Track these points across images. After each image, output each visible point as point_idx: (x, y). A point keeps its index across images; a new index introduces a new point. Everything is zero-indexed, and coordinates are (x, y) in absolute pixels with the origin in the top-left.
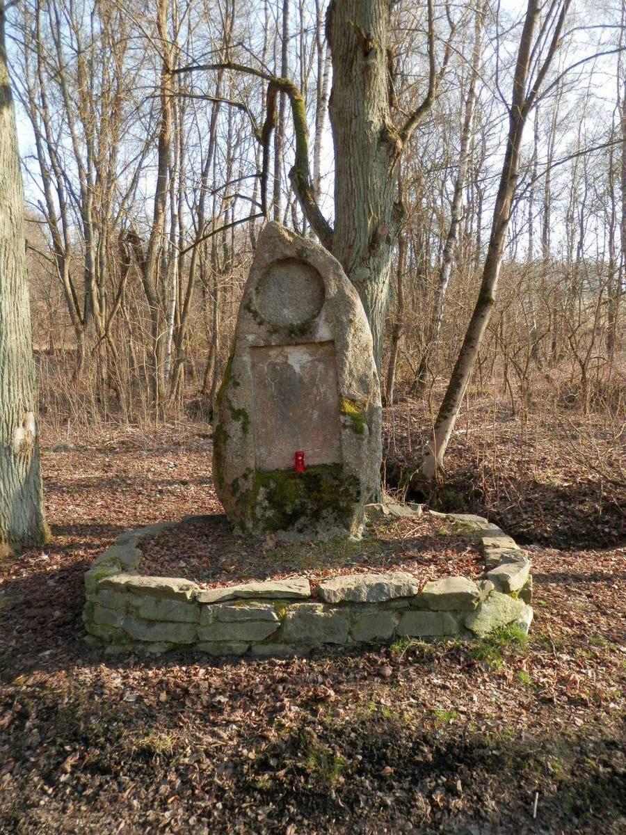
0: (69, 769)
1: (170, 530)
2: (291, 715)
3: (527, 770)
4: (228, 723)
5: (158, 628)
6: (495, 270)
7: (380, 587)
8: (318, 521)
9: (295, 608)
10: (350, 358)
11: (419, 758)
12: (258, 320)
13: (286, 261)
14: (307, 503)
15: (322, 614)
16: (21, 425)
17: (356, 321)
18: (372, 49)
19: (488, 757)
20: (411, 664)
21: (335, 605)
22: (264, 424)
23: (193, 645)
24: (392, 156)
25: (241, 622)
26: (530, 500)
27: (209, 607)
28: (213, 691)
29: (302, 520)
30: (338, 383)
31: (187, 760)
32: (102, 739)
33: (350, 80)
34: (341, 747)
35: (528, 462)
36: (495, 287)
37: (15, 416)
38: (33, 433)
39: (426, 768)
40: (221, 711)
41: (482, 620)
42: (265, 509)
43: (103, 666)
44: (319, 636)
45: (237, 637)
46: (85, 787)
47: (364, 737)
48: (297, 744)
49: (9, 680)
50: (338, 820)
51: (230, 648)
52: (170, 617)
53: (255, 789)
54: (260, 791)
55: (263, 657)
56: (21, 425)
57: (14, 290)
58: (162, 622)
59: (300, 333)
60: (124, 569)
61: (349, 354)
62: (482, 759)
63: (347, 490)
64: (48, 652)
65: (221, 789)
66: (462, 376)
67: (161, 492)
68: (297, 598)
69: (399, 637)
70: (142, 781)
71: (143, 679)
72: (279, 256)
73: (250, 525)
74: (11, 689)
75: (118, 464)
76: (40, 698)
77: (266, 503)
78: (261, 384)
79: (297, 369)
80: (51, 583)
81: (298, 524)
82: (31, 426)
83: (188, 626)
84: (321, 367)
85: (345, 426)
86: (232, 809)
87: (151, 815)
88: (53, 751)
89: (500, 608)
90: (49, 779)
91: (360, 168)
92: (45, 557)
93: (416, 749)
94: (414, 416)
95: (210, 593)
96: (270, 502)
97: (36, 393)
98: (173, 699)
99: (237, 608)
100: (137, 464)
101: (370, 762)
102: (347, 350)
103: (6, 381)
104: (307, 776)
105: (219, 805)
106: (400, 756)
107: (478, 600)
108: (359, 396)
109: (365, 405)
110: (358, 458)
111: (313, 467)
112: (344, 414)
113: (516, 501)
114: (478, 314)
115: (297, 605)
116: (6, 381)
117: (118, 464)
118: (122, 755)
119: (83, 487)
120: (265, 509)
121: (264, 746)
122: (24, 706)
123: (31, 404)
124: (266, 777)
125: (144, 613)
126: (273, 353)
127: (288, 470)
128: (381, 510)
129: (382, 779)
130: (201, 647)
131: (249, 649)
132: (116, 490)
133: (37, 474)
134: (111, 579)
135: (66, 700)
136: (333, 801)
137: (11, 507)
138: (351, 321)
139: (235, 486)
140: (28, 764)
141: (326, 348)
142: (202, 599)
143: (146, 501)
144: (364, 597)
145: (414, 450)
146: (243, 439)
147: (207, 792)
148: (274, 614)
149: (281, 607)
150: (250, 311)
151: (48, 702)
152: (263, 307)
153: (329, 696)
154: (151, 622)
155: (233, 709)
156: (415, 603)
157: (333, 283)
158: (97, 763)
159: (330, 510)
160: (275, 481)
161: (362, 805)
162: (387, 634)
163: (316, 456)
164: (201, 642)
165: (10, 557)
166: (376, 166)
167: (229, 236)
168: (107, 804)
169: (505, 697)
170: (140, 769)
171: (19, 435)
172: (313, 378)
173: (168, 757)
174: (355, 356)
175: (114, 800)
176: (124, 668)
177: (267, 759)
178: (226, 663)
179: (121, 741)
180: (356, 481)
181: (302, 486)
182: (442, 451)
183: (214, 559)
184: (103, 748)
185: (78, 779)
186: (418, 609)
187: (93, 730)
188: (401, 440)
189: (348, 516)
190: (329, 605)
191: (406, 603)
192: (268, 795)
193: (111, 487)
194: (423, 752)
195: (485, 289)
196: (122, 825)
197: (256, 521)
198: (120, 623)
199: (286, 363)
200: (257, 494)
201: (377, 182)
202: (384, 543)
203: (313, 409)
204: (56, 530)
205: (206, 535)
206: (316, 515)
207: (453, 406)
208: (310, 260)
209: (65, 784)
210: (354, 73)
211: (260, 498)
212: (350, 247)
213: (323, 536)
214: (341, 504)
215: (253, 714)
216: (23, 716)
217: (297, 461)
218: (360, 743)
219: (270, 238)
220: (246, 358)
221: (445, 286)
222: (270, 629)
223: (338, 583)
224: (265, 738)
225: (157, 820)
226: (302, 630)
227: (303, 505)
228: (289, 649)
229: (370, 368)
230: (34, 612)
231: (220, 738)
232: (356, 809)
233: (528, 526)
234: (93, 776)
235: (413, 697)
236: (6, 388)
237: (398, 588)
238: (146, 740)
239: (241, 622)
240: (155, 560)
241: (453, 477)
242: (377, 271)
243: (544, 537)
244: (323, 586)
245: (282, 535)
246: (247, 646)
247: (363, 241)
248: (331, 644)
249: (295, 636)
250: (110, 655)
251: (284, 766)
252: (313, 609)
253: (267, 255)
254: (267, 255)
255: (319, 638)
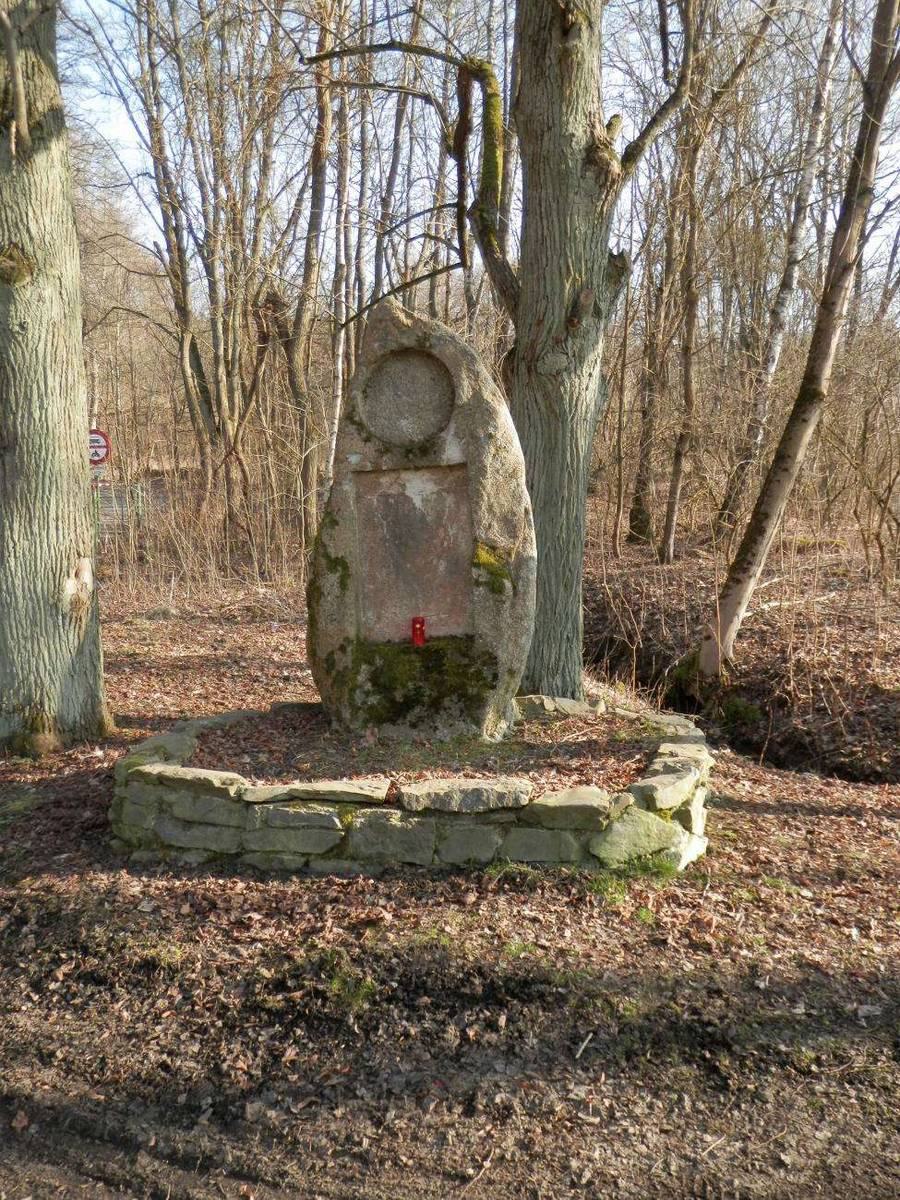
0: (61, 978)
1: (250, 719)
2: (330, 936)
3: (591, 1010)
4: (254, 940)
5: (196, 831)
6: (828, 345)
7: (477, 792)
8: (437, 712)
9: (364, 815)
10: (488, 487)
11: (467, 991)
12: (364, 435)
13: (403, 353)
14: (423, 686)
15: (399, 824)
16: (72, 575)
17: (499, 436)
18: (573, 24)
19: (551, 994)
20: (505, 893)
21: (417, 813)
22: (372, 578)
23: (238, 855)
24: (604, 184)
25: (293, 828)
26: (861, 714)
27: (256, 807)
28: (246, 907)
29: (417, 710)
30: (473, 522)
31: (194, 976)
32: (103, 949)
33: (543, 73)
34: (374, 971)
35: (869, 655)
36: (827, 372)
37: (65, 563)
38: (90, 587)
39: (471, 1001)
40: (248, 928)
41: (612, 844)
42: (367, 694)
43: (123, 872)
44: (394, 852)
45: (291, 847)
46: (74, 995)
47: (408, 964)
48: (324, 966)
49: (13, 882)
50: (347, 1045)
51: (282, 862)
52: (212, 817)
53: (263, 1009)
54: (269, 1011)
55: (320, 875)
56: (72, 575)
57: (66, 390)
58: (200, 824)
59: (420, 454)
60: (167, 758)
61: (488, 482)
62: (542, 996)
63: (479, 672)
64: (64, 856)
65: (225, 1007)
66: (767, 516)
67: (286, 679)
68: (369, 802)
69: (500, 860)
70: (139, 994)
71: (167, 889)
72: (394, 346)
73: (347, 714)
74: (13, 892)
75: (234, 639)
76: (43, 903)
77: (369, 686)
78: (368, 522)
79: (418, 502)
80: (93, 782)
81: (411, 717)
82: (87, 577)
83: (232, 830)
84: (450, 500)
85: (478, 583)
86: (233, 1027)
87: (140, 1026)
88: (47, 957)
89: (641, 830)
90: (37, 986)
91: (554, 206)
92: (99, 753)
93: (467, 980)
94: (702, 579)
95: (260, 789)
96: (375, 684)
97: (92, 531)
98: (197, 912)
99: (291, 810)
100: (261, 640)
101: (405, 990)
102: (484, 476)
103: (53, 515)
104: (325, 999)
105: (220, 1023)
106: (444, 987)
107: (608, 817)
108: (503, 541)
109: (509, 555)
110: (496, 628)
111: (438, 638)
112: (478, 565)
113: (841, 713)
114: (797, 418)
115: (368, 811)
116: (53, 515)
117: (234, 639)
118: (121, 967)
119: (181, 667)
120: (367, 694)
121: (286, 966)
122: (23, 910)
123: (88, 546)
124: (280, 997)
125: (178, 811)
126: (385, 480)
127: (405, 641)
128: (542, 704)
129: (413, 1008)
130: (248, 858)
131: (307, 864)
132: (224, 675)
133: (95, 644)
134: (141, 768)
135: (72, 906)
136: (349, 1027)
137: (58, 684)
138: (490, 436)
139: (330, 662)
140: (17, 970)
141: (457, 473)
142: (249, 797)
143: (261, 691)
144: (455, 806)
145: (694, 633)
146: (341, 598)
147: (208, 1009)
148: (337, 821)
149: (347, 812)
150: (353, 422)
151: (51, 906)
152: (372, 415)
153: (382, 919)
154: (188, 824)
155: (264, 926)
156: (523, 816)
157: (466, 383)
158: (92, 972)
159: (455, 698)
160: (381, 657)
161: (380, 1032)
162: (486, 855)
163: (441, 624)
164: (248, 852)
165: (55, 751)
166: (578, 202)
167: (441, 290)
168: (94, 1014)
169: (609, 936)
170: (139, 981)
171: (70, 587)
172: (439, 516)
173: (172, 970)
174: (497, 487)
175: (103, 1011)
176: (149, 877)
177: (284, 978)
178: (274, 878)
179: (126, 951)
180: (492, 660)
181: (418, 664)
182: (732, 635)
183: (288, 755)
184: (103, 958)
185: (69, 987)
186: (529, 825)
187: (94, 938)
188: (674, 617)
189: (479, 707)
190: (408, 813)
191: (512, 817)
192: (276, 1015)
193: (218, 671)
194: (472, 983)
195: (811, 377)
196: (106, 1035)
197: (355, 709)
198: (151, 822)
199: (403, 494)
200: (358, 672)
201: (581, 226)
202: (530, 747)
203: (439, 557)
204: (123, 721)
205: (295, 728)
206: (436, 705)
207: (750, 563)
208: (435, 352)
209: (54, 992)
210: (548, 62)
211: (361, 678)
212: (540, 322)
213: (443, 733)
214: (470, 691)
215: (287, 934)
216: (22, 921)
217: (414, 630)
218: (400, 970)
219: (381, 321)
220: (348, 487)
221: (773, 369)
222: (333, 839)
223: (424, 787)
224: (289, 958)
225: (146, 1033)
226: (373, 844)
227: (418, 689)
228: (356, 867)
229: (520, 503)
230: (63, 812)
231: (239, 955)
232: (372, 1036)
233: (853, 753)
234: (85, 985)
235: (490, 928)
236: (53, 525)
237: (501, 796)
238: (153, 952)
239: (293, 828)
240: (212, 753)
241: (746, 674)
242: (580, 358)
243: (876, 772)
244: (404, 789)
245: (389, 730)
246: (303, 860)
247: (557, 316)
248: (411, 864)
249: (364, 851)
250: (135, 862)
251: (302, 987)
252: (386, 817)
253: (376, 345)
254: (376, 345)
255: (394, 855)
